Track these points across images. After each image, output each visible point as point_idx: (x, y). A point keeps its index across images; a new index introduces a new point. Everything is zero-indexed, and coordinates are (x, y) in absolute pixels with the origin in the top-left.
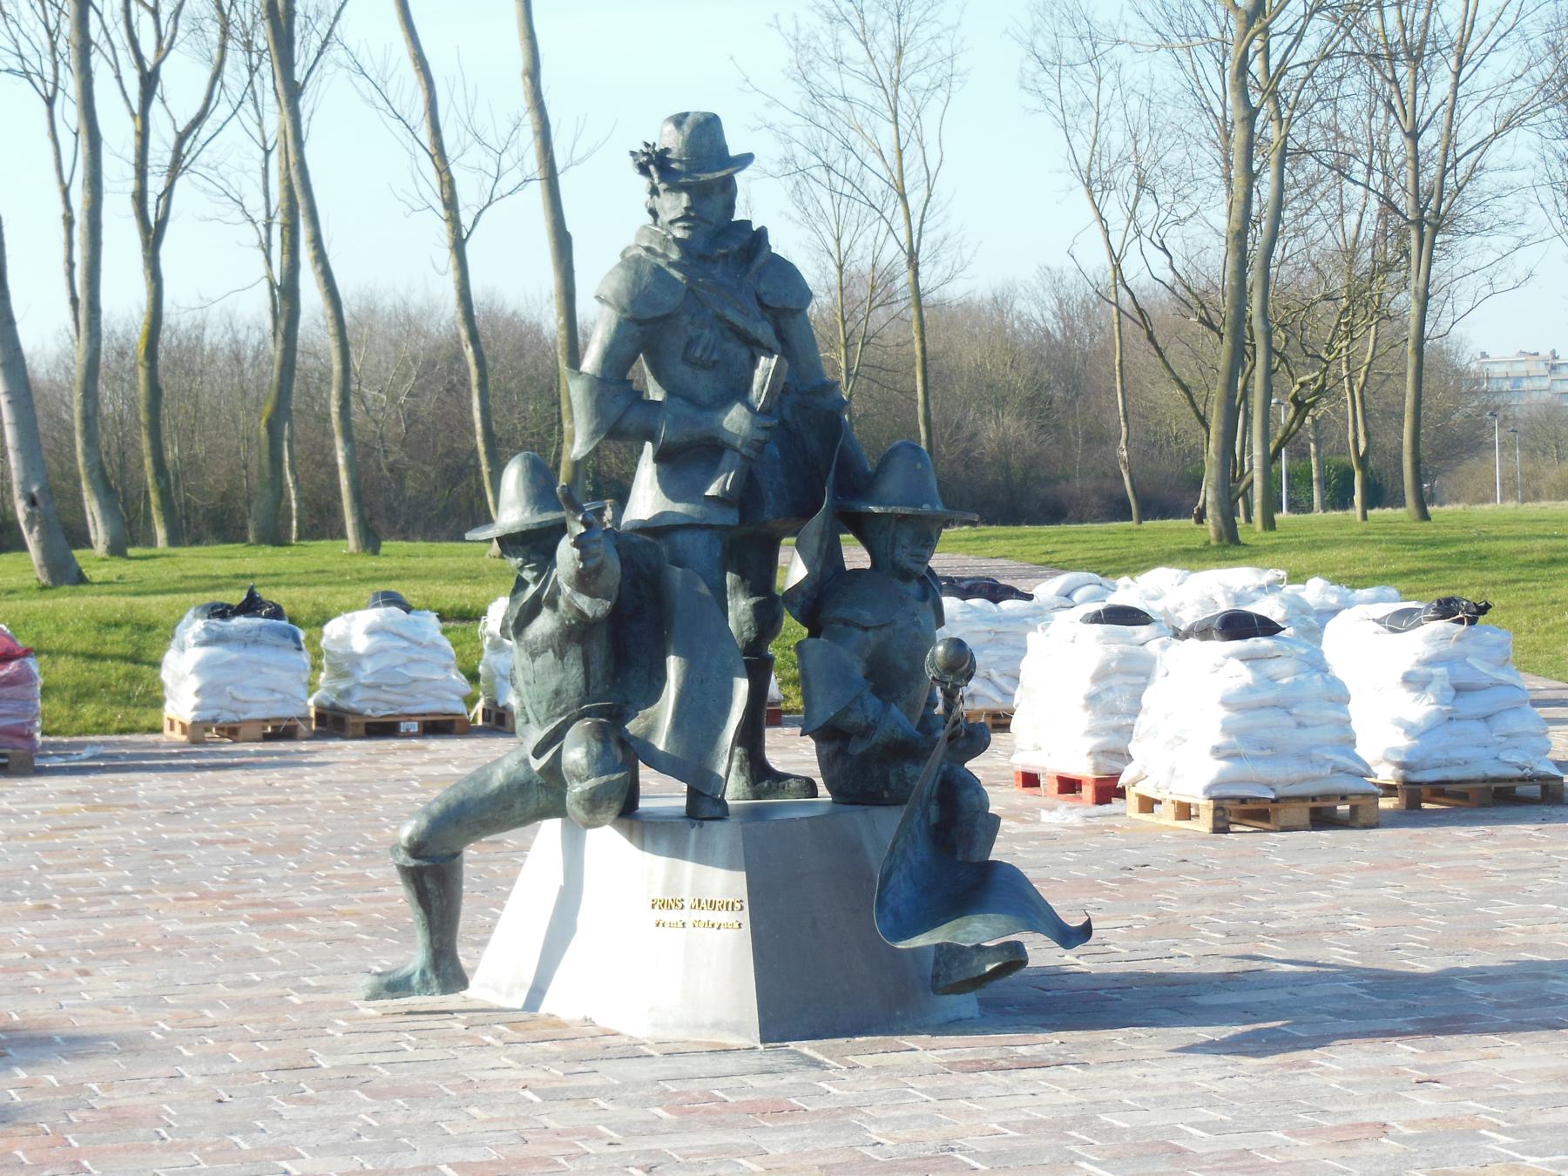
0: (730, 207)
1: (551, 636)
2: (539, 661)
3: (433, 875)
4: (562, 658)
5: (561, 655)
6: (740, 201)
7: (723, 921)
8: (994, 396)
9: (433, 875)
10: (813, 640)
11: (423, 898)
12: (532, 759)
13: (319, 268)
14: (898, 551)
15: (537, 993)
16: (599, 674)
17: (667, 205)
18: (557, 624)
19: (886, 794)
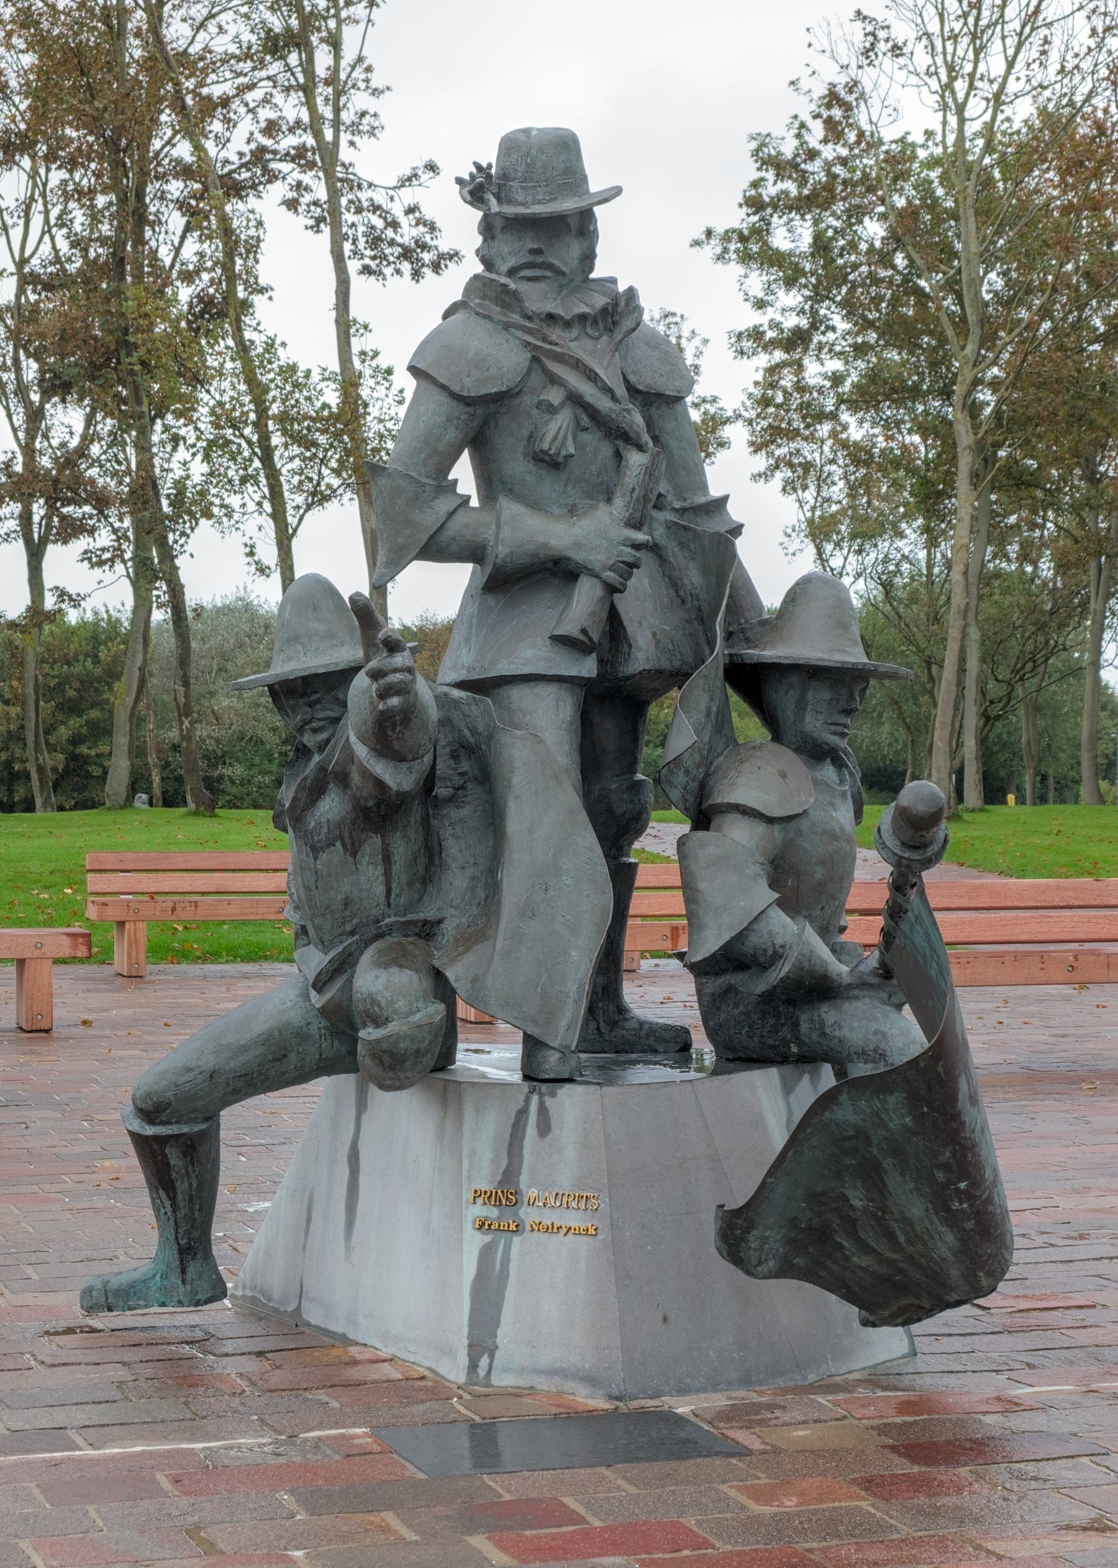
0: (588, 258)
1: (339, 825)
2: (324, 857)
3: (178, 1154)
4: (354, 854)
5: (353, 850)
6: (601, 249)
7: (574, 1224)
8: (974, 1154)
9: (178, 1154)
10: (700, 834)
11: (161, 1177)
12: (313, 993)
13: (601, 980)
14: (809, 717)
15: (481, 1345)
16: (404, 878)
17: (506, 250)
18: (348, 807)
19: (794, 1049)
